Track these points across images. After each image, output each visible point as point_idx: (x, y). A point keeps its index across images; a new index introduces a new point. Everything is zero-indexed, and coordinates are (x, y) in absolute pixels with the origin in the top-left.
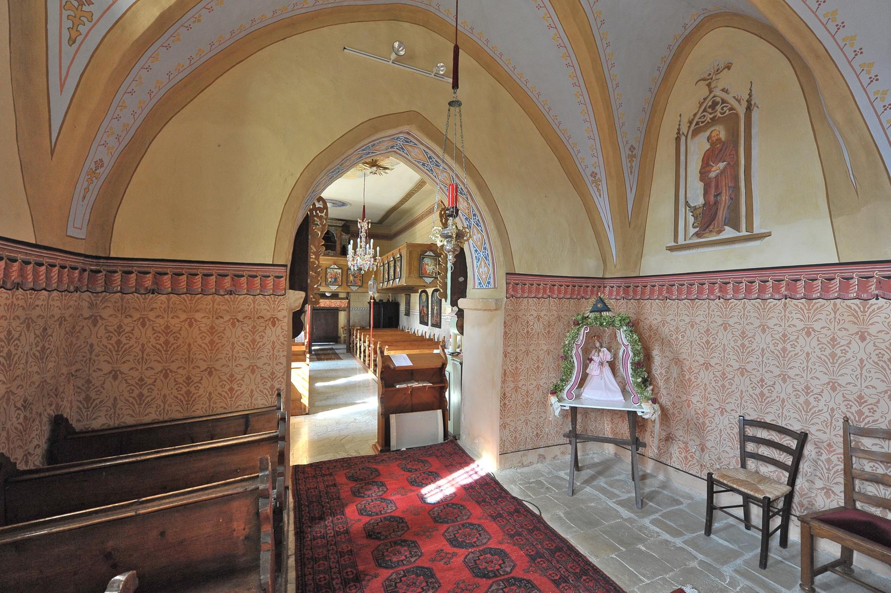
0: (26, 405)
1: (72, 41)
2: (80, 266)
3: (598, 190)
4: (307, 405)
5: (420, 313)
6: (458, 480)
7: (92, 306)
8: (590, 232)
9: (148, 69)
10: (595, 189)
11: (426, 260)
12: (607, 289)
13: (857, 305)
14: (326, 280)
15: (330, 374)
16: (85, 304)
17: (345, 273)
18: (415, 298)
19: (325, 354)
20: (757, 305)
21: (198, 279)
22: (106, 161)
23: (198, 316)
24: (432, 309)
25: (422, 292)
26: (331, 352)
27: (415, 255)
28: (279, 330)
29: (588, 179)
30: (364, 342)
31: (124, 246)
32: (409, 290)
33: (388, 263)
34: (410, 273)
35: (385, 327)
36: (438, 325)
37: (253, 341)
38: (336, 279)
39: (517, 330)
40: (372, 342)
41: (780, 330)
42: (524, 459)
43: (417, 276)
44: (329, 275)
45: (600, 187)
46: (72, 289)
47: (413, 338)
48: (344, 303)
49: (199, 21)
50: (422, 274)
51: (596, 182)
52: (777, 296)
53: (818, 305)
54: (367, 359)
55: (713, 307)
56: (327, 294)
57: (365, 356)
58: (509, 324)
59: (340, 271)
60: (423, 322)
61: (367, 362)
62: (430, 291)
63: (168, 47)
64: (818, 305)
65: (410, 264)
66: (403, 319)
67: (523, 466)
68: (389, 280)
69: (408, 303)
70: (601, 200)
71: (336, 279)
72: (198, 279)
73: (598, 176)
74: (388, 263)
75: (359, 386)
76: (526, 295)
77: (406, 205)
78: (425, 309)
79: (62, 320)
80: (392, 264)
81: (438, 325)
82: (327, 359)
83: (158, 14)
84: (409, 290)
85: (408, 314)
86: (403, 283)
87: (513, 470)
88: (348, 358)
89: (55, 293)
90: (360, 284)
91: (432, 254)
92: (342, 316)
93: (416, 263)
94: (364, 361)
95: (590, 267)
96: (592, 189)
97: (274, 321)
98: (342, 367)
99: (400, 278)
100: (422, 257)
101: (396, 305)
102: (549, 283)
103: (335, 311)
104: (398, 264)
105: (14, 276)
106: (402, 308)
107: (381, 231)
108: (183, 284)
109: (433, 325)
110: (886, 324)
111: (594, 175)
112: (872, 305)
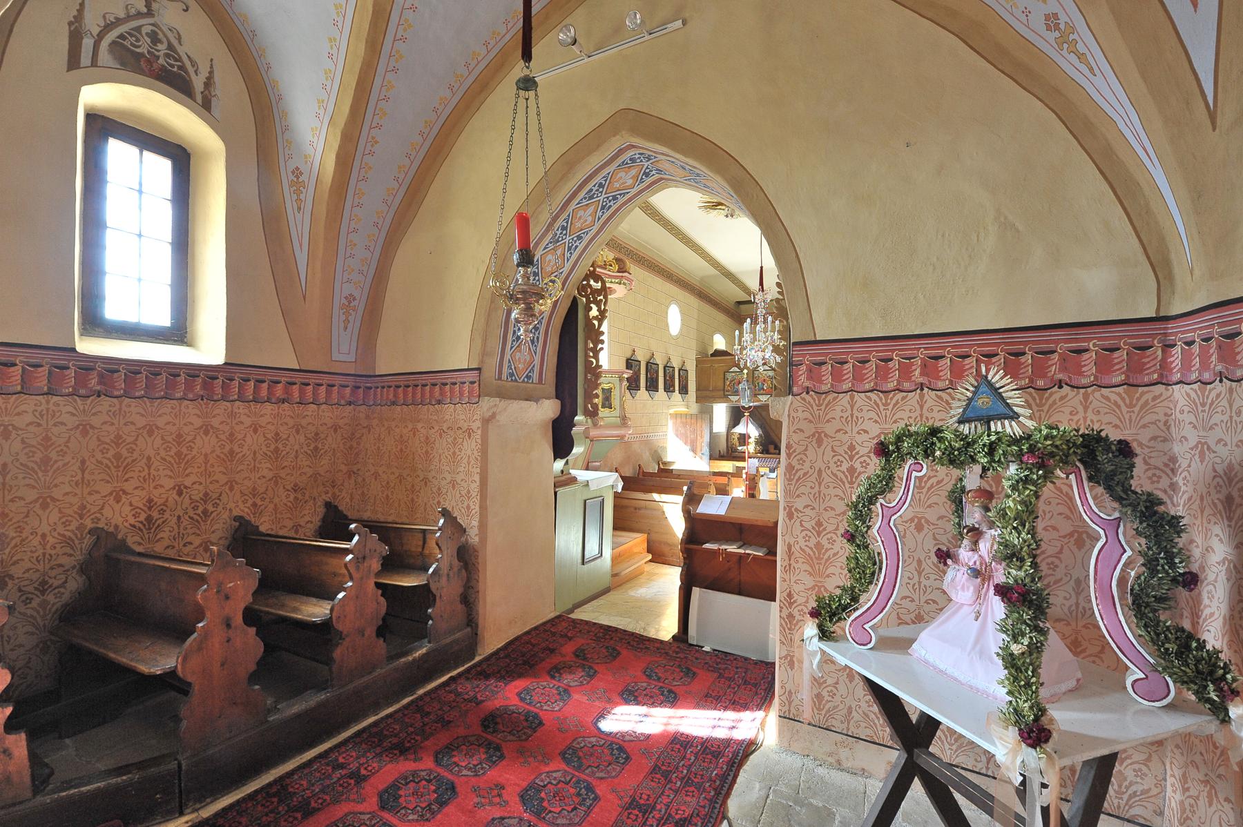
0: (296, 489)
1: (299, 209)
2: (393, 384)
3: (1081, 57)
6: (684, 721)
7: (368, 417)
8: (1089, 184)
9: (360, 205)
10: (1073, 58)
12: (1177, 351)
13: (1119, 394)
16: (362, 416)
20: (1193, 395)
21: (323, 389)
22: (357, 294)
23: (419, 426)
28: (474, 444)
29: (1046, 41)
31: (386, 364)
37: (454, 453)
39: (819, 464)
41: (75, 500)
42: (844, 753)
45: (1081, 47)
46: (343, 402)
49: (376, 142)
51: (1066, 39)
52: (82, 392)
53: (1149, 396)
55: (1095, 404)
58: (800, 449)
63: (365, 179)
64: (1149, 396)
67: (839, 766)
70: (1098, 80)
72: (323, 389)
73: (1063, 19)
76: (845, 387)
79: (336, 428)
83: (334, 157)
87: (809, 763)
89: (324, 406)
95: (1095, 286)
96: (1068, 63)
97: (470, 432)
102: (922, 353)
105: (264, 393)
108: (296, 395)
110: (34, 560)
111: (1052, 21)
112: (1143, 394)
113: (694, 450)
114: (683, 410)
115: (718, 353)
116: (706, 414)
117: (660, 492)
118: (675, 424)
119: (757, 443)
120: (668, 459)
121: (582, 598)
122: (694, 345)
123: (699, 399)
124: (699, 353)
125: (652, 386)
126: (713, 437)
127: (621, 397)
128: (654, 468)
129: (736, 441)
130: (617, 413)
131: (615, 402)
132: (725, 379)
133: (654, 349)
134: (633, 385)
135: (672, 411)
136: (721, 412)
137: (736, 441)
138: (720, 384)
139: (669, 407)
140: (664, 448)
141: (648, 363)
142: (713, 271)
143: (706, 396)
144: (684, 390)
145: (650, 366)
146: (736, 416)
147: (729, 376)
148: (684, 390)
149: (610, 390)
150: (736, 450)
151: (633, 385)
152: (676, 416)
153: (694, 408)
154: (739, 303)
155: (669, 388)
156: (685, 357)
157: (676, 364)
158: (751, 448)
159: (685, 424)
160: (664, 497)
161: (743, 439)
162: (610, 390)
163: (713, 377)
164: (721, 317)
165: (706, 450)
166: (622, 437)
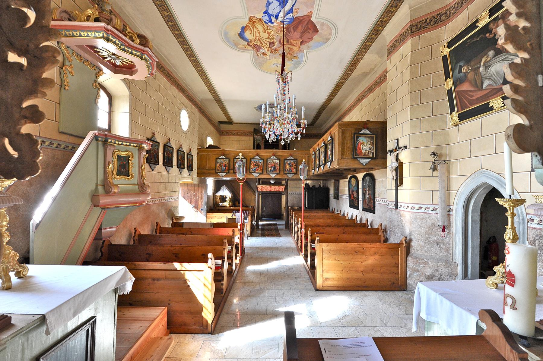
4: (210, 322)
5: (350, 197)
11: (361, 139)
14: (267, 169)
15: (268, 254)
17: (282, 163)
18: (344, 184)
19: (268, 230)
24: (364, 194)
25: (351, 178)
26: (273, 227)
27: (348, 135)
30: (298, 224)
32: (337, 175)
33: (319, 150)
34: (343, 155)
35: (317, 208)
36: (371, 209)
38: (275, 168)
40: (303, 227)
43: (350, 156)
44: (269, 165)
47: (343, 222)
48: (281, 188)
50: (356, 155)
54: (299, 241)
56: (272, 182)
57: (298, 236)
59: (278, 161)
60: (353, 204)
61: (299, 244)
62: (360, 176)
65: (342, 144)
66: (333, 203)
68: (320, 166)
69: (337, 189)
71: (275, 168)
74: (319, 150)
75: (289, 276)
77: (335, 101)
78: (355, 194)
80: (323, 150)
81: (371, 209)
82: (269, 235)
84: (337, 175)
85: (337, 197)
86: (335, 165)
88: (286, 235)
90: (295, 171)
91: (367, 132)
92: (284, 198)
93: (349, 143)
94: (298, 240)
98: (278, 245)
99: (331, 161)
100: (355, 137)
101: (327, 190)
103: (279, 195)
104: (329, 147)
106: (332, 192)
107: (314, 131)
109: (364, 209)
113: (196, 207)
114: (189, 181)
115: (210, 147)
116: (203, 184)
117: (181, 261)
118: (183, 190)
119: (230, 201)
120: (180, 215)
121: (85, 353)
122: (197, 140)
123: (199, 175)
124: (199, 145)
125: (168, 163)
126: (208, 197)
127: (140, 166)
128: (168, 225)
129: (218, 200)
130: (135, 180)
131: (133, 168)
132: (216, 163)
133: (170, 136)
134: (152, 159)
135: (181, 182)
136: (210, 182)
137: (218, 200)
138: (213, 165)
139: (180, 179)
140: (176, 208)
141: (165, 146)
142: (210, 96)
143: (203, 173)
144: (190, 168)
145: (167, 147)
146: (218, 185)
147: (219, 161)
148: (190, 168)
149: (127, 158)
150: (218, 205)
151: (152, 159)
152: (184, 185)
153: (196, 180)
154: (221, 123)
155: (180, 166)
156: (190, 146)
157: (185, 149)
158: (227, 204)
159: (190, 191)
160: (186, 266)
161: (223, 199)
162: (127, 158)
163: (207, 163)
164: (211, 128)
165: (204, 207)
166: (140, 204)
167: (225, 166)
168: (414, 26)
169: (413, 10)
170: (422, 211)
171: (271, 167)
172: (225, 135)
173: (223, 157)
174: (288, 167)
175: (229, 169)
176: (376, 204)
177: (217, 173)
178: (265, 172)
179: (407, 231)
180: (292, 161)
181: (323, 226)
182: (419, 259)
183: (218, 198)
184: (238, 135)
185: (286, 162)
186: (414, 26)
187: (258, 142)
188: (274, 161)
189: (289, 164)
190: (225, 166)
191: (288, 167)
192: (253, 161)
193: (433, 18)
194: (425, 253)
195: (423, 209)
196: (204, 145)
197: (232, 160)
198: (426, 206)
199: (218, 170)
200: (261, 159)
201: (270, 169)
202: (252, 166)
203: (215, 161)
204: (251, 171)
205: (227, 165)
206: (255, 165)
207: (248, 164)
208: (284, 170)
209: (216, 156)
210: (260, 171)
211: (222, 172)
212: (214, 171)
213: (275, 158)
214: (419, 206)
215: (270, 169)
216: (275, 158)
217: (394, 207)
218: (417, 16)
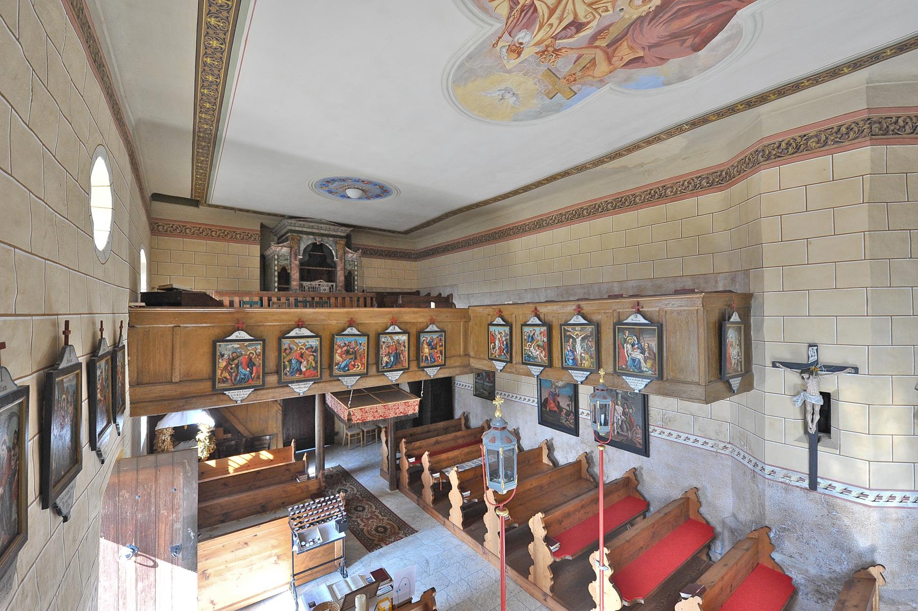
14: (378, 362)
17: (413, 340)
44: (383, 351)
59: (404, 338)
71: (397, 356)
132: (214, 356)
138: (202, 366)
147: (226, 349)
167: (250, 363)
168: (875, 123)
169: (874, 88)
170: (895, 503)
171: (388, 354)
172: (166, 233)
173: (243, 335)
174: (426, 350)
175: (265, 374)
176: (652, 440)
177: (218, 393)
178: (373, 370)
179: (863, 542)
180: (435, 336)
181: (575, 511)
182: (900, 604)
183: (167, 437)
184: (212, 238)
185: (422, 339)
186: (875, 123)
187: (284, 263)
188: (396, 337)
189: (429, 344)
190: (250, 363)
191: (426, 350)
192: (339, 341)
193: (908, 120)
194: (901, 588)
195: (898, 499)
196: (136, 289)
197: (272, 344)
198: (904, 494)
199: (225, 380)
200: (363, 335)
201: (385, 359)
202: (337, 358)
203: (206, 349)
204: (336, 372)
205: (258, 361)
206: (347, 352)
207: (326, 351)
208: (418, 358)
209: (216, 332)
210: (360, 369)
211: (239, 385)
212: (207, 386)
213: (397, 330)
214: (889, 493)
215: (385, 359)
216: (397, 330)
217: (806, 484)
218: (878, 103)
